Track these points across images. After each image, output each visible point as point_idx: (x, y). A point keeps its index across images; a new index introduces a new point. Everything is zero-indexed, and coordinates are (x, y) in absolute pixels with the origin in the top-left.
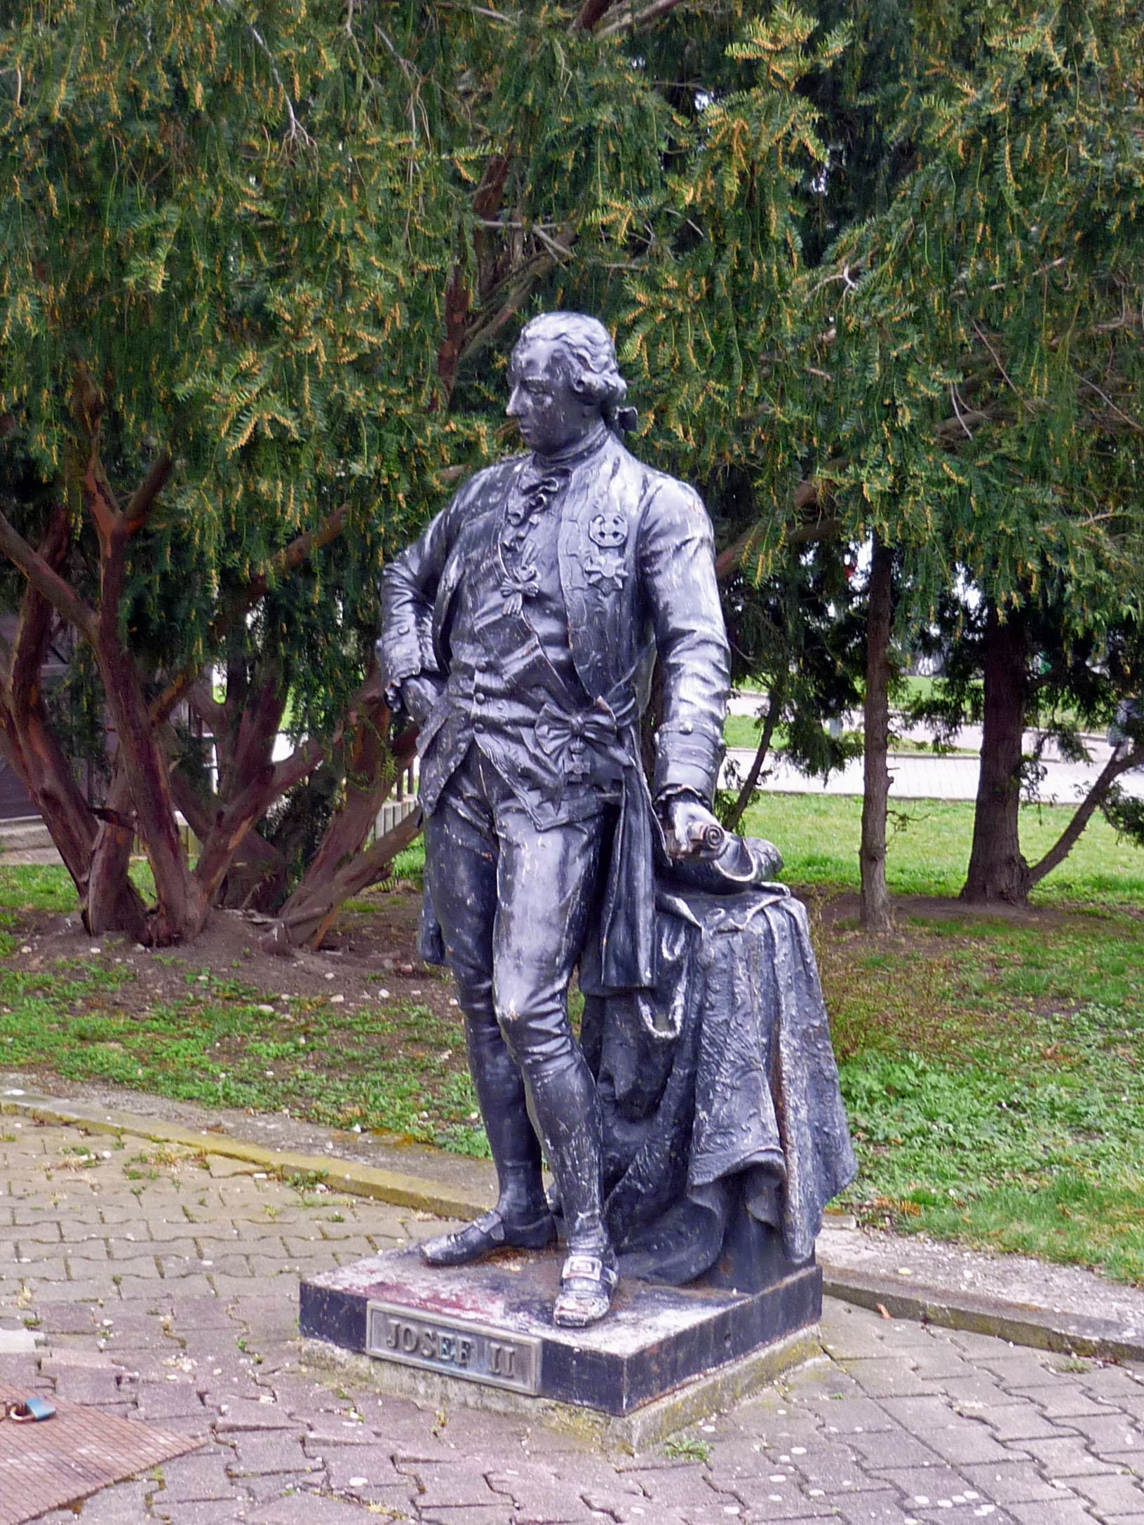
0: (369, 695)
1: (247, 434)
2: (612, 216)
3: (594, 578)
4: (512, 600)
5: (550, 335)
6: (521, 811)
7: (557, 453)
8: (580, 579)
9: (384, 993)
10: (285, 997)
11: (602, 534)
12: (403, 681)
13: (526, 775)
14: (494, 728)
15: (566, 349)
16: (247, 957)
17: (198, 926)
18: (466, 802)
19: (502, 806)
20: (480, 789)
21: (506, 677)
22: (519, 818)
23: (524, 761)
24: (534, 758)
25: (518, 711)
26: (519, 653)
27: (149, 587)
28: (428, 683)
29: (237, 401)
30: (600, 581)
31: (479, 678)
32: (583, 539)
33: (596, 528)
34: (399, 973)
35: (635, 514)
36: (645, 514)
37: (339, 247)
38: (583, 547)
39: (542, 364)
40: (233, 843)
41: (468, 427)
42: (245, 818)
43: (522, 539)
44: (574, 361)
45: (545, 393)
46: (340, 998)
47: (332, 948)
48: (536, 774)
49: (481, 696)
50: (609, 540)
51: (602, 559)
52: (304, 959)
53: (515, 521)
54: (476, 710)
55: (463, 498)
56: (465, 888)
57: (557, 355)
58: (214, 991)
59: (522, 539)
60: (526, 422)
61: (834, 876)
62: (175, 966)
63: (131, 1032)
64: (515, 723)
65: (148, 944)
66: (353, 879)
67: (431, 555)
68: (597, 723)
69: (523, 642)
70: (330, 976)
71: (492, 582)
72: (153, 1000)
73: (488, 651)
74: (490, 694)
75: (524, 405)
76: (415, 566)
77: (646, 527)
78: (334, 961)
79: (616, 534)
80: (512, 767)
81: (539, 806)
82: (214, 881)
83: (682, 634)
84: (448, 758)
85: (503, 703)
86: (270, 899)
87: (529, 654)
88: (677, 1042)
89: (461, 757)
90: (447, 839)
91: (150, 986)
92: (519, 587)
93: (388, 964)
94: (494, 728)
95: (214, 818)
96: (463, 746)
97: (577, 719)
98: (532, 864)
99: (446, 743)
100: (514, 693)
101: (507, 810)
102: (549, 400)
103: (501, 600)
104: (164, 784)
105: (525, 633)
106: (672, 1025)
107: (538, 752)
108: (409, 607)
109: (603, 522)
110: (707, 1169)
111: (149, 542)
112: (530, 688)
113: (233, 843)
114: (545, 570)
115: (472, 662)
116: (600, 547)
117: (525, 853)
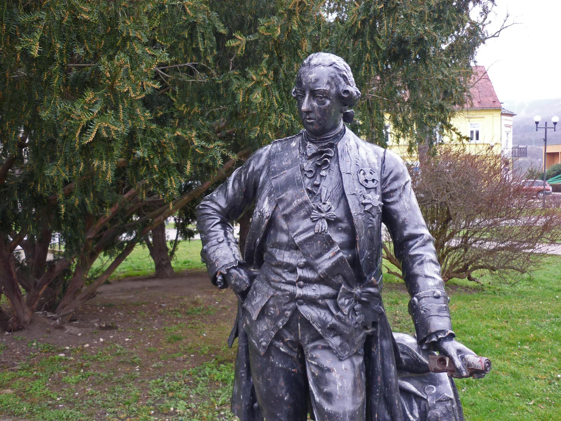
0: (88, 237)
1: (93, 135)
2: (238, 43)
3: (368, 208)
4: (319, 223)
5: (327, 63)
6: (329, 348)
7: (322, 137)
8: (359, 208)
9: (101, 340)
10: (68, 348)
11: (366, 181)
12: (228, 270)
14: (311, 301)
15: (337, 72)
16: (49, 332)
17: (28, 323)
18: (285, 344)
19: (311, 345)
20: (296, 336)
21: (320, 271)
22: (326, 353)
23: (331, 320)
24: (338, 318)
25: (325, 290)
26: (327, 256)
27: (8, 207)
28: (242, 271)
29: (85, 118)
30: (371, 209)
31: (299, 272)
32: (356, 184)
33: (362, 178)
34: (101, 328)
35: (378, 168)
36: (383, 168)
37: (128, 43)
38: (358, 189)
39: (325, 80)
40: (41, 293)
41: (185, 133)
42: (45, 284)
43: (318, 186)
44: (341, 79)
45: (327, 98)
46: (87, 345)
47: (75, 320)
48: (339, 327)
49: (301, 283)
50: (370, 184)
51: (369, 196)
52: (69, 329)
53: (310, 175)
54: (299, 292)
55: (258, 162)
56: (284, 391)
57: (333, 75)
58: (40, 349)
59: (318, 186)
60: (312, 115)
61: (193, 267)
62: (22, 340)
63: (13, 379)
64: (324, 297)
65: (10, 331)
66: (83, 299)
67: (235, 195)
68: (370, 292)
69: (329, 249)
70: (80, 334)
71: (303, 213)
72: (17, 358)
73: (305, 255)
74: (307, 282)
75: (312, 105)
76: (222, 203)
77: (385, 176)
78: (79, 326)
79: (373, 180)
80: (323, 323)
81: (341, 345)
82: (34, 306)
83: (414, 237)
84: (275, 319)
85: (315, 286)
86: (52, 307)
87: (334, 256)
89: (287, 319)
90: (273, 365)
91: (14, 350)
92: (323, 215)
93: (96, 325)
94: (311, 301)
95: (32, 285)
96: (289, 313)
97: (357, 291)
98: (343, 382)
100: (321, 281)
101: (315, 348)
102: (328, 102)
103: (312, 224)
104: (15, 277)
105: (330, 243)
107: (339, 314)
108: (219, 226)
109: (364, 174)
111: (6, 189)
112: (334, 277)
113: (41, 293)
114: (336, 204)
115: (293, 261)
116: (367, 189)
117: (335, 375)
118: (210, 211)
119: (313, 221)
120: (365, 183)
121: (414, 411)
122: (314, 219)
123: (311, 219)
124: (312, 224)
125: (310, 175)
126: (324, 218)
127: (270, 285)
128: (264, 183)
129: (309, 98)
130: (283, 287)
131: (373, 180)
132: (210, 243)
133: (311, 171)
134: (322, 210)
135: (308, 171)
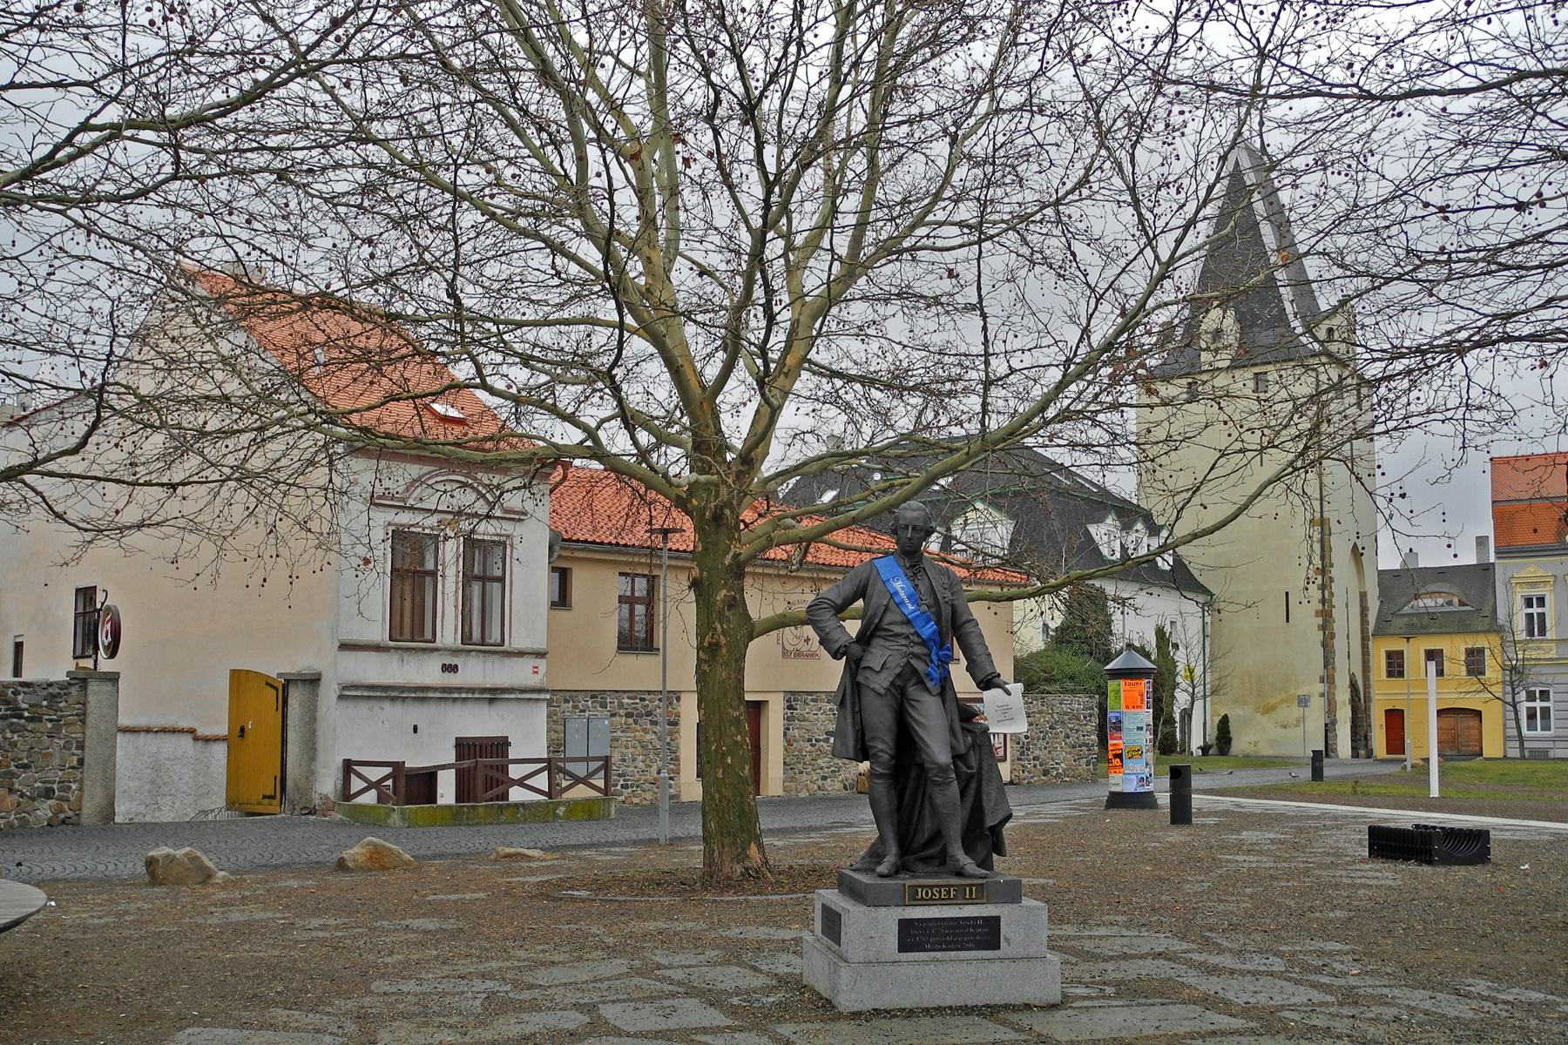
13: (928, 675)
25: (925, 651)
88: (972, 775)
100: (923, 643)
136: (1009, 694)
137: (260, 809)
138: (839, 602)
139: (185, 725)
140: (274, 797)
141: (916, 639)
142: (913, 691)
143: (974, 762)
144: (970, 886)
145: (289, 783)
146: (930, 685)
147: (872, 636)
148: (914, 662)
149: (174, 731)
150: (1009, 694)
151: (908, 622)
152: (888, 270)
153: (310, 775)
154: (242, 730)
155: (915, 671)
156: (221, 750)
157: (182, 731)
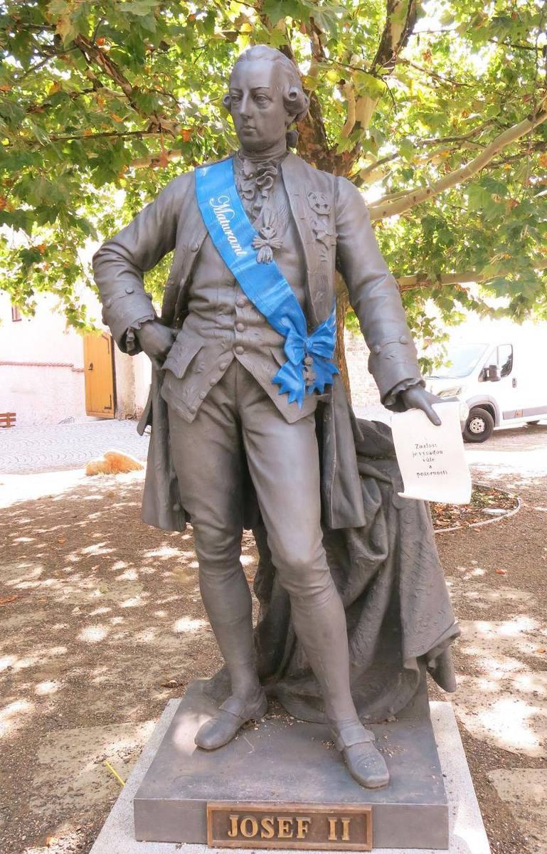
11: (317, 205)
25: (272, 337)
50: (322, 210)
53: (250, 197)
88: (383, 564)
92: (267, 242)
97: (309, 341)
99: (201, 364)
100: (268, 322)
106: (376, 550)
110: (414, 647)
118: (114, 257)
119: (255, 250)
120: (315, 208)
121: (371, 559)
122: (256, 247)
123: (253, 246)
124: (253, 252)
125: (250, 197)
126: (267, 244)
127: (200, 334)
128: (99, 492)
129: (248, 99)
130: (218, 333)
131: (326, 206)
132: (116, 295)
133: (250, 192)
134: (265, 236)
135: (246, 192)
136: (435, 421)
137: (104, 415)
138: (135, 248)
139: (67, 362)
140: (110, 408)
141: (246, 314)
142: (254, 416)
143: (385, 541)
144: (339, 816)
145: (118, 400)
146: (281, 402)
147: (185, 312)
148: (246, 360)
149: (62, 366)
150: (435, 421)
151: (235, 283)
152: (495, 160)
153: (131, 394)
154: (91, 365)
155: (250, 379)
156: (82, 376)
157: (66, 366)
